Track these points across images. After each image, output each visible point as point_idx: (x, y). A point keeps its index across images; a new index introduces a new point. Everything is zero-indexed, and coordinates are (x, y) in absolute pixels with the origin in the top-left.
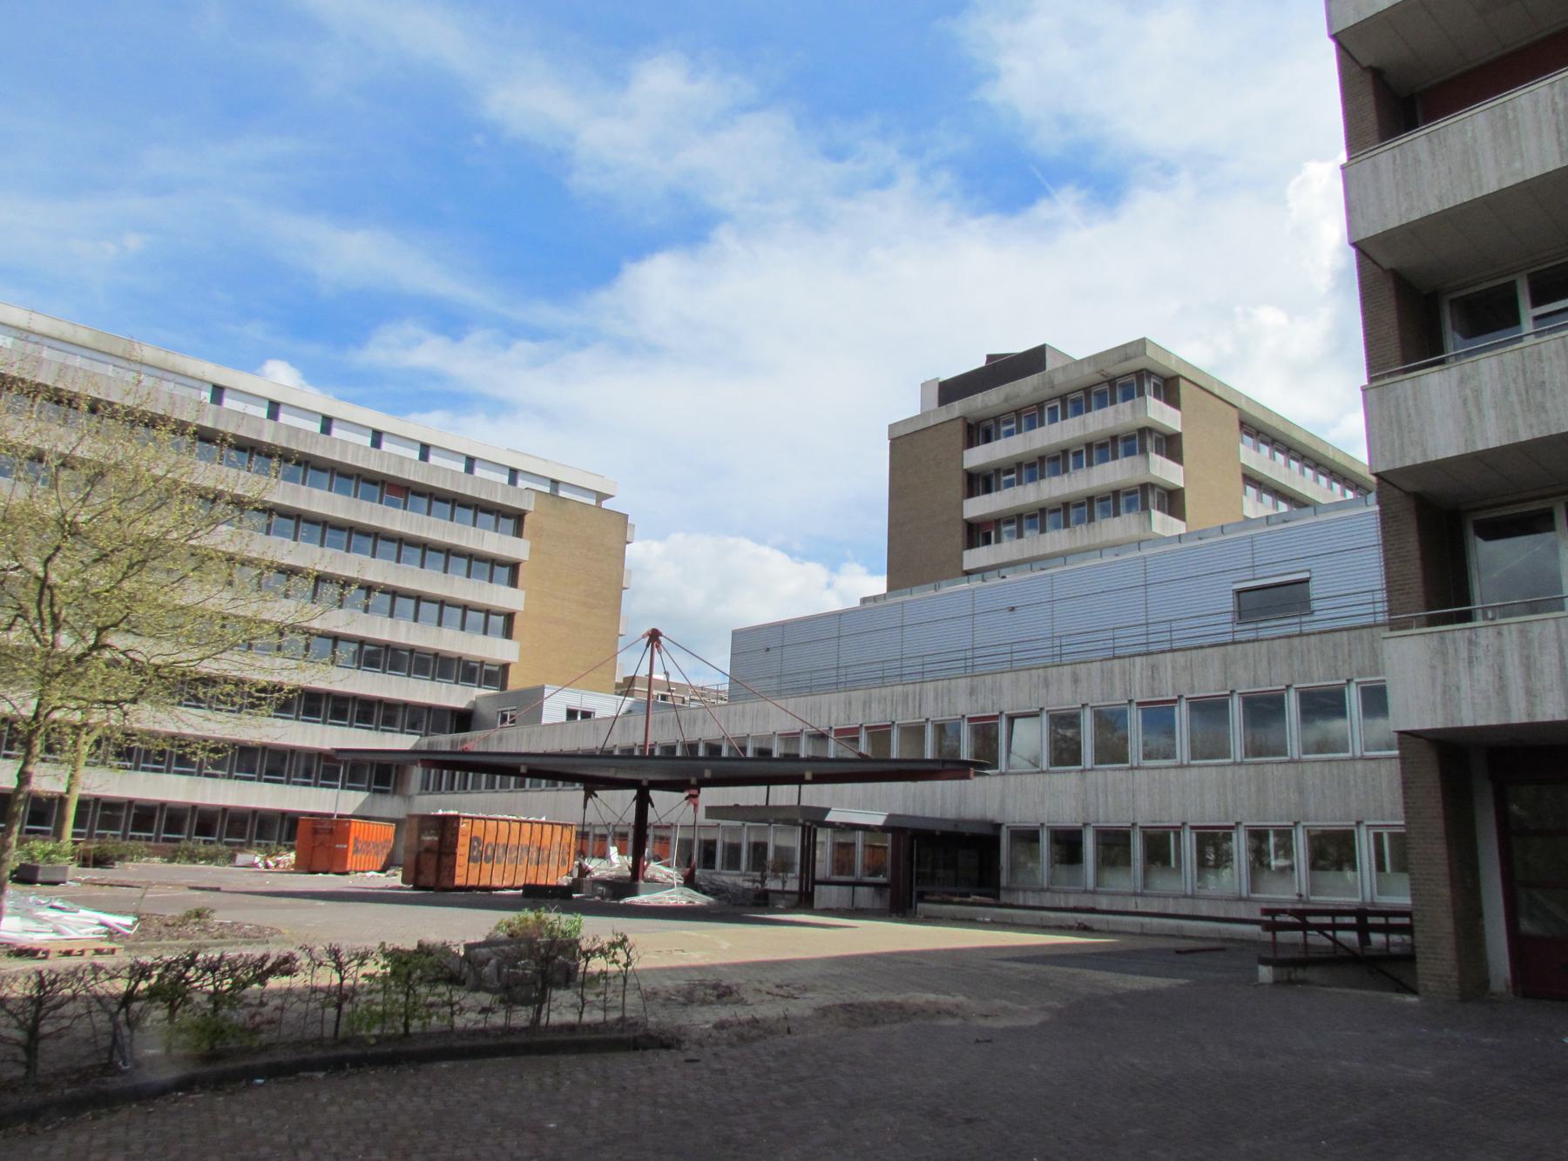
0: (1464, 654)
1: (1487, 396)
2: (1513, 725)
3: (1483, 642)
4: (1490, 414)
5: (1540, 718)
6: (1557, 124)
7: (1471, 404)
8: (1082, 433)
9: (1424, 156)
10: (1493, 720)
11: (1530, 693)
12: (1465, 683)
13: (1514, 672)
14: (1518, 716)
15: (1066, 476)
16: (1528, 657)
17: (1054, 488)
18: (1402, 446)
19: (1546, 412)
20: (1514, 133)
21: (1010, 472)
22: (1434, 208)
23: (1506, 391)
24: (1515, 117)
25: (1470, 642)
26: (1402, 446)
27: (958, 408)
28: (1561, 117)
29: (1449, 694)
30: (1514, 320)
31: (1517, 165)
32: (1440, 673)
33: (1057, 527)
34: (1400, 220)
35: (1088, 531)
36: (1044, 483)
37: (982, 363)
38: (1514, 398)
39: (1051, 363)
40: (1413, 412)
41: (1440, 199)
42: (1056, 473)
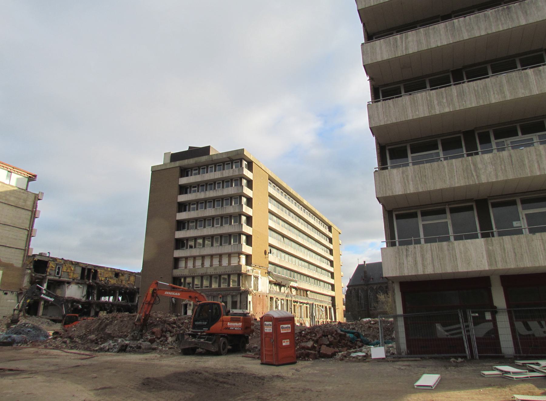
0: (405, 253)
1: (410, 177)
2: (448, 273)
3: (410, 250)
4: (411, 183)
5: (426, 273)
6: (428, 104)
7: (405, 179)
8: (221, 177)
9: (391, 105)
10: (413, 273)
11: (423, 265)
12: (405, 262)
13: (419, 259)
14: (420, 272)
15: (215, 191)
16: (423, 255)
17: (211, 194)
18: (386, 190)
19: (426, 184)
20: (416, 104)
21: (195, 187)
22: (394, 121)
23: (415, 177)
24: (417, 99)
25: (407, 250)
26: (386, 190)
27: (178, 164)
28: (429, 102)
29: (401, 265)
30: (406, 156)
31: (417, 113)
32: (398, 259)
33: (210, 207)
34: (385, 123)
35: (221, 210)
36: (207, 193)
37: (187, 149)
38: (417, 178)
39: (211, 153)
40: (389, 180)
41: (396, 119)
42: (211, 189)
